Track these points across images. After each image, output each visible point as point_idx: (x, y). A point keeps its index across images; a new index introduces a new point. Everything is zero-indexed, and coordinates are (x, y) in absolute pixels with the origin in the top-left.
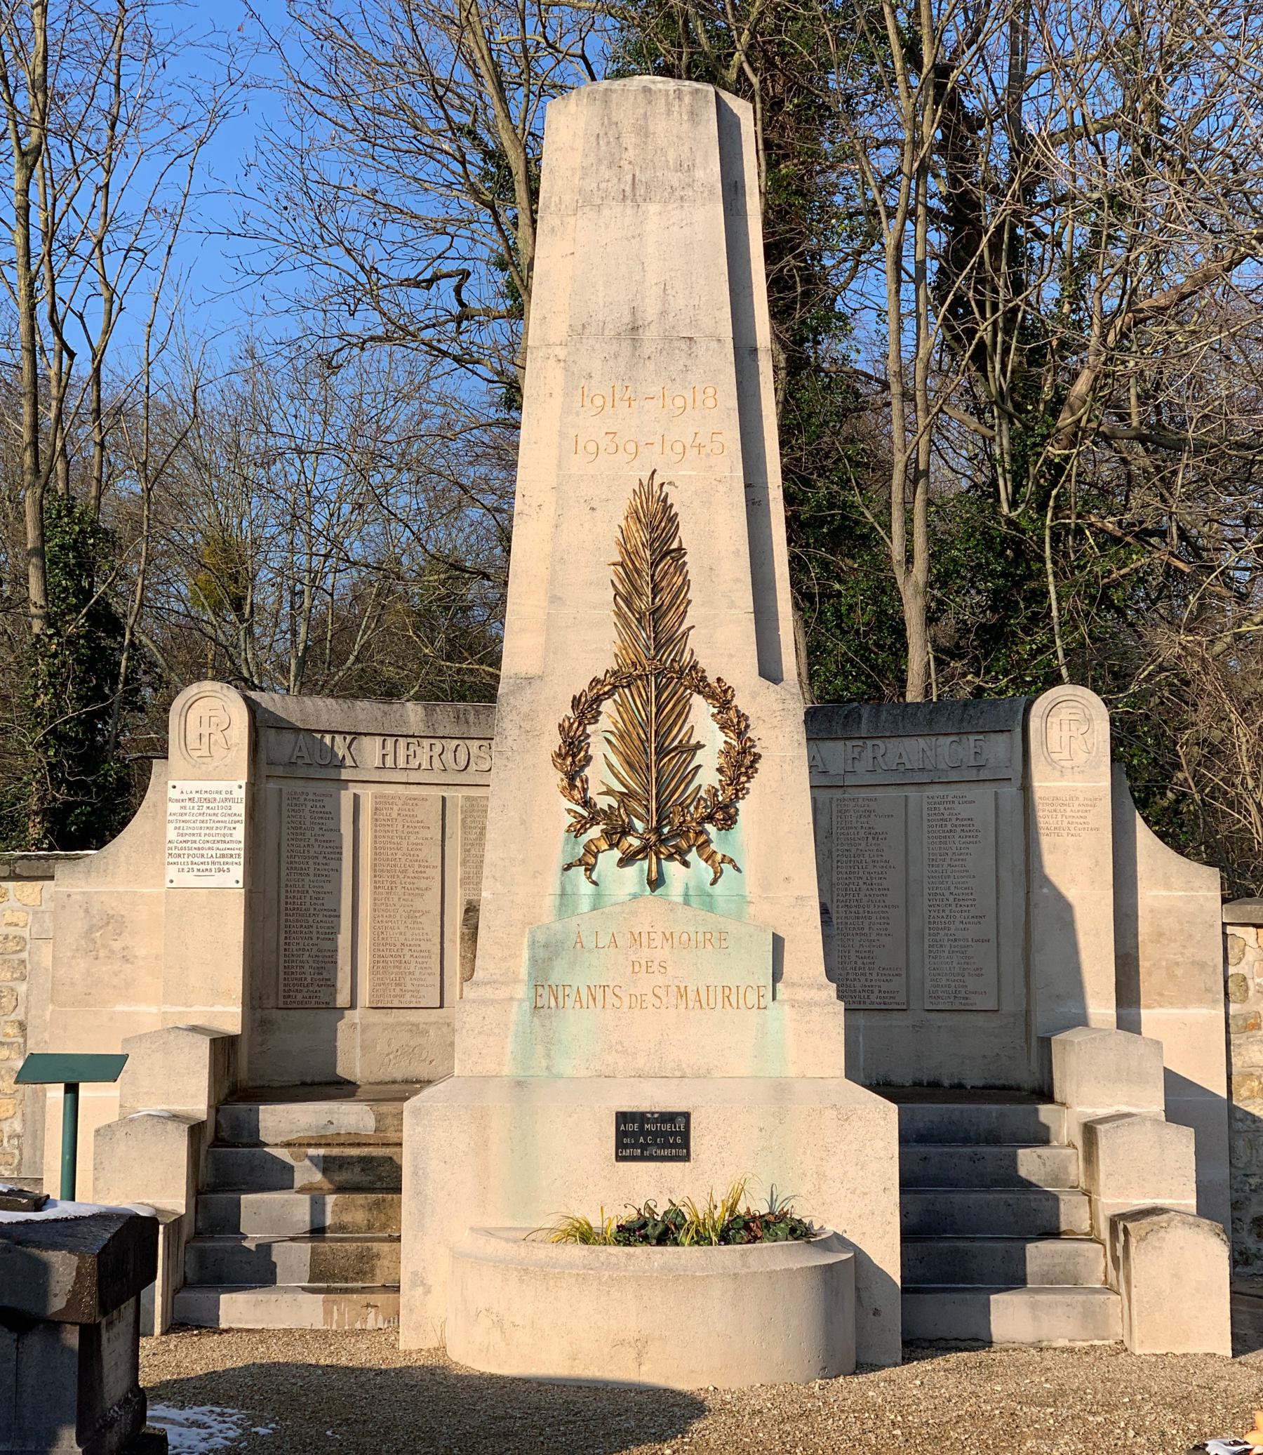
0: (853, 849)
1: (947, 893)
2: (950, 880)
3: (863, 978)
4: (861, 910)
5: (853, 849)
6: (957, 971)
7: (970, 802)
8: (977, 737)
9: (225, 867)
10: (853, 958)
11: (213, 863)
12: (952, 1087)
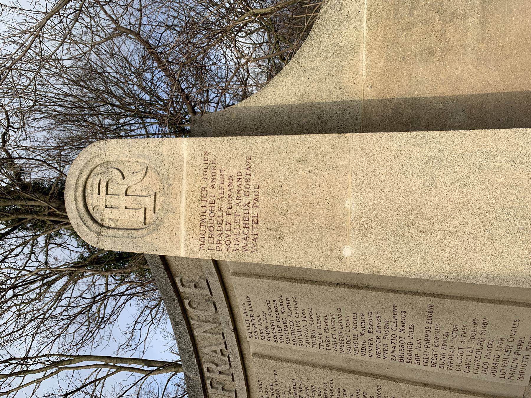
1: (361, 339)
6: (475, 346)
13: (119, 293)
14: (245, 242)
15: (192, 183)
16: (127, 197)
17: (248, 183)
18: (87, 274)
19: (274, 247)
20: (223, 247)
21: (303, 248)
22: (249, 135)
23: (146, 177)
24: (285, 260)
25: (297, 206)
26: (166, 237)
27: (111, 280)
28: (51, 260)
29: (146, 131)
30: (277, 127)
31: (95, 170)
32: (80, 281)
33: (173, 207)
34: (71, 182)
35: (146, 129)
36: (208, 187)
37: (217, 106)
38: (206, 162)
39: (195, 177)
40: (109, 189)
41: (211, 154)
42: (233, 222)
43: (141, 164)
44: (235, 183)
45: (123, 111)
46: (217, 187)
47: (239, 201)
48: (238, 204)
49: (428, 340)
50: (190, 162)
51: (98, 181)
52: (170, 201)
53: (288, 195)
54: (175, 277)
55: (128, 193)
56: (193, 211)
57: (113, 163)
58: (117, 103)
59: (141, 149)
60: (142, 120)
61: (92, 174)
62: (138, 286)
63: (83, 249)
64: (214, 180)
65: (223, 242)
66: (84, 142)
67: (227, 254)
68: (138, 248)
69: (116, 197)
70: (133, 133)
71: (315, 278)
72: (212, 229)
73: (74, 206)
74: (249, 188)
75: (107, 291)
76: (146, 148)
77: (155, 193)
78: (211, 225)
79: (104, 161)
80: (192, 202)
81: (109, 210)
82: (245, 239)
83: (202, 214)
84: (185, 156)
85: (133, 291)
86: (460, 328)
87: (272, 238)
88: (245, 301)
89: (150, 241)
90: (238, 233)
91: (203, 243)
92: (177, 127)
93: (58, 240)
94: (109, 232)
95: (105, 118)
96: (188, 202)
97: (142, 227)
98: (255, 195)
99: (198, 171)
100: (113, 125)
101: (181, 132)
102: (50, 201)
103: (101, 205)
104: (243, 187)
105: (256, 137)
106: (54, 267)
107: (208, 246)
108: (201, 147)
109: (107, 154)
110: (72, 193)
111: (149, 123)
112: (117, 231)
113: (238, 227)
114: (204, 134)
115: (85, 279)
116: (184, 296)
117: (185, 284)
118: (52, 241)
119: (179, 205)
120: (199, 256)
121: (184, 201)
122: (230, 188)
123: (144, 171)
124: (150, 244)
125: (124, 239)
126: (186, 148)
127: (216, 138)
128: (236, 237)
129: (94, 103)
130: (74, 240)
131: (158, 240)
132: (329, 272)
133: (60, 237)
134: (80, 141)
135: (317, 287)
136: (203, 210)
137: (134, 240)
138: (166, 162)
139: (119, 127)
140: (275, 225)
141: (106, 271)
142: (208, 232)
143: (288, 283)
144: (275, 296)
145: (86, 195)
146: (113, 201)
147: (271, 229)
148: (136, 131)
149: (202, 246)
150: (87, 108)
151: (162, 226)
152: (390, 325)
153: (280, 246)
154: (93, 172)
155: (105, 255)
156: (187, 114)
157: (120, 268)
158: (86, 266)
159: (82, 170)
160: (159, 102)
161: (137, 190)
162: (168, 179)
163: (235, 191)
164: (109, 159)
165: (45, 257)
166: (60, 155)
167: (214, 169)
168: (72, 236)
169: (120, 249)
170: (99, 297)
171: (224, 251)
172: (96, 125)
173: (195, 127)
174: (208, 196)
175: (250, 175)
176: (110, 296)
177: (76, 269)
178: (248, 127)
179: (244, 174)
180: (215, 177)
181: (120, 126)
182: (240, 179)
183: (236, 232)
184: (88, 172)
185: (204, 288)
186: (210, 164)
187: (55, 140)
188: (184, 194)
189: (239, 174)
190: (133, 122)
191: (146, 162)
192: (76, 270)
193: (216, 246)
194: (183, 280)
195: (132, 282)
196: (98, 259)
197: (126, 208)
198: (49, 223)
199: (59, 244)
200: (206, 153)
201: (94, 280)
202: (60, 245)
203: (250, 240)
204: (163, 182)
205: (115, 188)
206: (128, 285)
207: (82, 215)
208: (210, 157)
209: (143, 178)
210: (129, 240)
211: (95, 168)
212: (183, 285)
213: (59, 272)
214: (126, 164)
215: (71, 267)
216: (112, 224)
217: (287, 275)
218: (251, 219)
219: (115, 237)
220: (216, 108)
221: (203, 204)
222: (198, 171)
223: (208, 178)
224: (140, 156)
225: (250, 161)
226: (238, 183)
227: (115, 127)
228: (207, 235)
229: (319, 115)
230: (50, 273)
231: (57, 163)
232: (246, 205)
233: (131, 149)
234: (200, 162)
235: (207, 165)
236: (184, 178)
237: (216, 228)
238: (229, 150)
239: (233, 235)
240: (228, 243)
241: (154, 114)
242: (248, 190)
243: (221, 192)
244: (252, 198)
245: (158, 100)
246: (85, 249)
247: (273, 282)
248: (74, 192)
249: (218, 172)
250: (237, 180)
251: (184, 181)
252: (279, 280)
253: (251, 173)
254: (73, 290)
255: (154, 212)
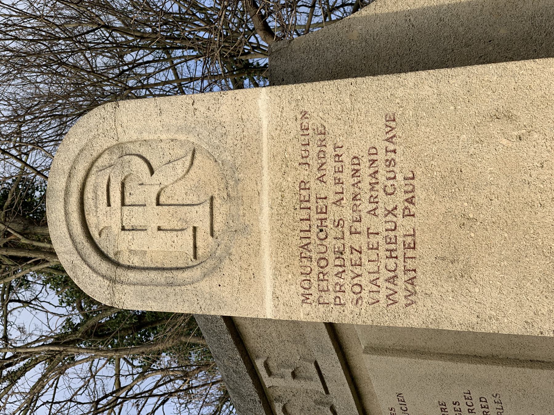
13: (141, 394)
14: (391, 286)
15: (280, 174)
16: (160, 207)
17: (391, 168)
18: (80, 358)
19: (451, 294)
20: (348, 297)
21: (513, 295)
22: (388, 71)
23: (192, 168)
24: (475, 320)
25: (497, 209)
26: (236, 282)
27: (125, 367)
28: (14, 334)
29: (176, 74)
30: (445, 50)
31: (100, 161)
32: (70, 370)
33: (247, 223)
34: (57, 183)
35: (175, 70)
36: (312, 180)
37: (312, 12)
38: (306, 132)
39: (285, 161)
40: (127, 194)
41: (315, 115)
42: (364, 248)
43: (182, 144)
44: (365, 170)
45: (130, 38)
46: (330, 180)
47: (374, 206)
48: (373, 212)
50: (275, 134)
51: (106, 182)
52: (241, 213)
53: (476, 188)
54: (254, 357)
55: (162, 200)
56: (285, 230)
57: (131, 146)
58: (118, 24)
59: (181, 115)
60: (168, 53)
61: (94, 169)
62: (177, 378)
63: (71, 309)
64: (324, 167)
65: (347, 288)
66: (60, 105)
67: (357, 310)
68: (186, 304)
69: (141, 209)
70: (152, 81)
71: (539, 354)
72: (323, 263)
73: (65, 230)
74: (395, 178)
75: (120, 389)
76: (191, 113)
77: (212, 199)
78: (322, 256)
79: (115, 143)
80: (282, 211)
81: (129, 235)
82: (392, 280)
83: (303, 234)
84: (265, 123)
85: (170, 387)
87: (446, 276)
89: (207, 290)
90: (376, 269)
91: (308, 292)
92: (235, 62)
93: (25, 294)
94: (132, 276)
95: (97, 54)
96: (275, 212)
97: (191, 264)
98: (406, 192)
99: (290, 150)
100: (114, 67)
101: (240, 72)
102: (5, 221)
103: (114, 226)
104: (381, 177)
105: (403, 75)
106: (19, 344)
107: (317, 296)
108: (294, 104)
109: (120, 129)
110: (60, 206)
111: (180, 57)
112: (145, 274)
113: (374, 257)
114: (296, 77)
115: (78, 367)
116: (273, 394)
117: (274, 371)
118: (13, 296)
119: (257, 220)
120: (302, 317)
121: (266, 210)
122: (356, 180)
123: (189, 158)
124: (207, 296)
125: (158, 289)
126: (265, 107)
127: (322, 83)
128: (373, 277)
129: (75, 28)
130: (52, 293)
131: (221, 288)
133: (27, 289)
134: (54, 102)
135: (546, 373)
136: (305, 226)
137: (177, 289)
138: (229, 137)
139: (124, 71)
140: (452, 250)
141: (116, 351)
142: (316, 270)
143: (481, 367)
145: (86, 208)
146: (135, 217)
147: (443, 259)
148: (157, 76)
149: (306, 298)
150: (65, 39)
151: (227, 261)
153: (465, 292)
154: (96, 164)
155: (111, 318)
156: (253, 32)
157: (140, 343)
158: (79, 341)
159: (76, 161)
160: (198, 14)
161: (179, 193)
162: (235, 169)
163: (365, 185)
164: (124, 138)
165: (3, 328)
166: (19, 133)
167: (322, 144)
168: (48, 286)
169: (155, 307)
170: (104, 402)
171: (350, 306)
172: (83, 70)
173: (279, 63)
174: (313, 199)
175: (394, 151)
176: (125, 399)
177: (62, 349)
178: (384, 54)
179: (381, 152)
180: (324, 161)
181: (126, 68)
182: (374, 161)
183: (371, 267)
184: (87, 165)
185: (311, 379)
186: (312, 134)
187: (10, 105)
188: (265, 198)
189: (373, 151)
190: (150, 58)
191: (192, 139)
192: (59, 350)
193: (333, 295)
194: (270, 364)
195: (167, 369)
196: (99, 327)
197: (159, 229)
198: (7, 261)
199: (26, 302)
200: (304, 114)
201: (94, 369)
202: (27, 303)
203: (400, 282)
204: (224, 177)
205: (137, 192)
206: (159, 376)
207: (79, 246)
208: (313, 122)
209: (188, 171)
210: (169, 290)
211: (99, 156)
212: (270, 373)
213: (31, 354)
214: (154, 145)
215: (50, 345)
216: (136, 261)
217: (479, 351)
218: (400, 240)
219: (142, 284)
220: (311, 15)
221: (304, 214)
222: (290, 150)
223: (311, 163)
224: (179, 130)
225: (393, 124)
226: (372, 170)
227: (117, 71)
228: (314, 275)
229: (533, 18)
230: (14, 356)
231: (15, 147)
232: (389, 212)
233: (164, 116)
234: (294, 133)
235: (307, 137)
236: (265, 164)
237: (331, 261)
238: (349, 105)
239: (366, 274)
240: (357, 289)
241: (190, 39)
242: (392, 182)
243: (338, 189)
244: (400, 197)
245: (195, 11)
246: (74, 308)
247: (450, 364)
248: (63, 203)
249: (329, 150)
250: (368, 164)
251: (265, 171)
252: (464, 361)
253: (397, 147)
254: (56, 387)
255: (212, 235)
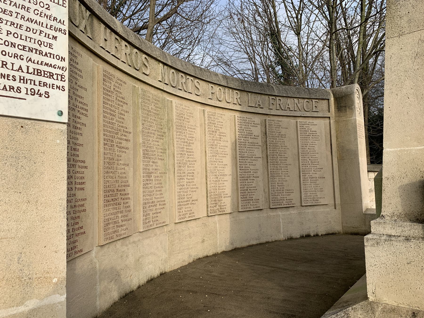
0: (274, 141)
1: (308, 159)
2: (309, 155)
3: (280, 194)
4: (278, 166)
5: (274, 141)
6: (313, 190)
7: (315, 125)
8: (315, 101)
9: (43, 90)
10: (277, 186)
11: (23, 80)
12: (314, 236)
49: (312, 178)
86: (319, 185)
88: (315, 123)
132: (232, 154)
136: (44, 25)
144: (318, 134)
152: (316, 168)
